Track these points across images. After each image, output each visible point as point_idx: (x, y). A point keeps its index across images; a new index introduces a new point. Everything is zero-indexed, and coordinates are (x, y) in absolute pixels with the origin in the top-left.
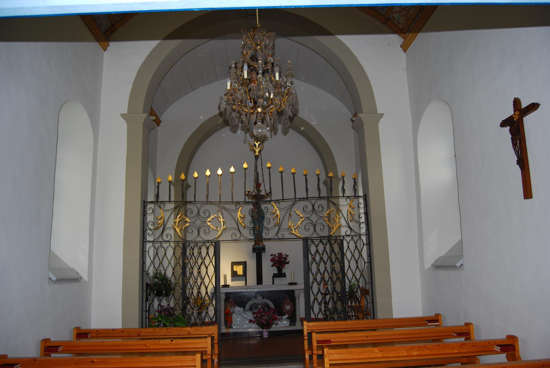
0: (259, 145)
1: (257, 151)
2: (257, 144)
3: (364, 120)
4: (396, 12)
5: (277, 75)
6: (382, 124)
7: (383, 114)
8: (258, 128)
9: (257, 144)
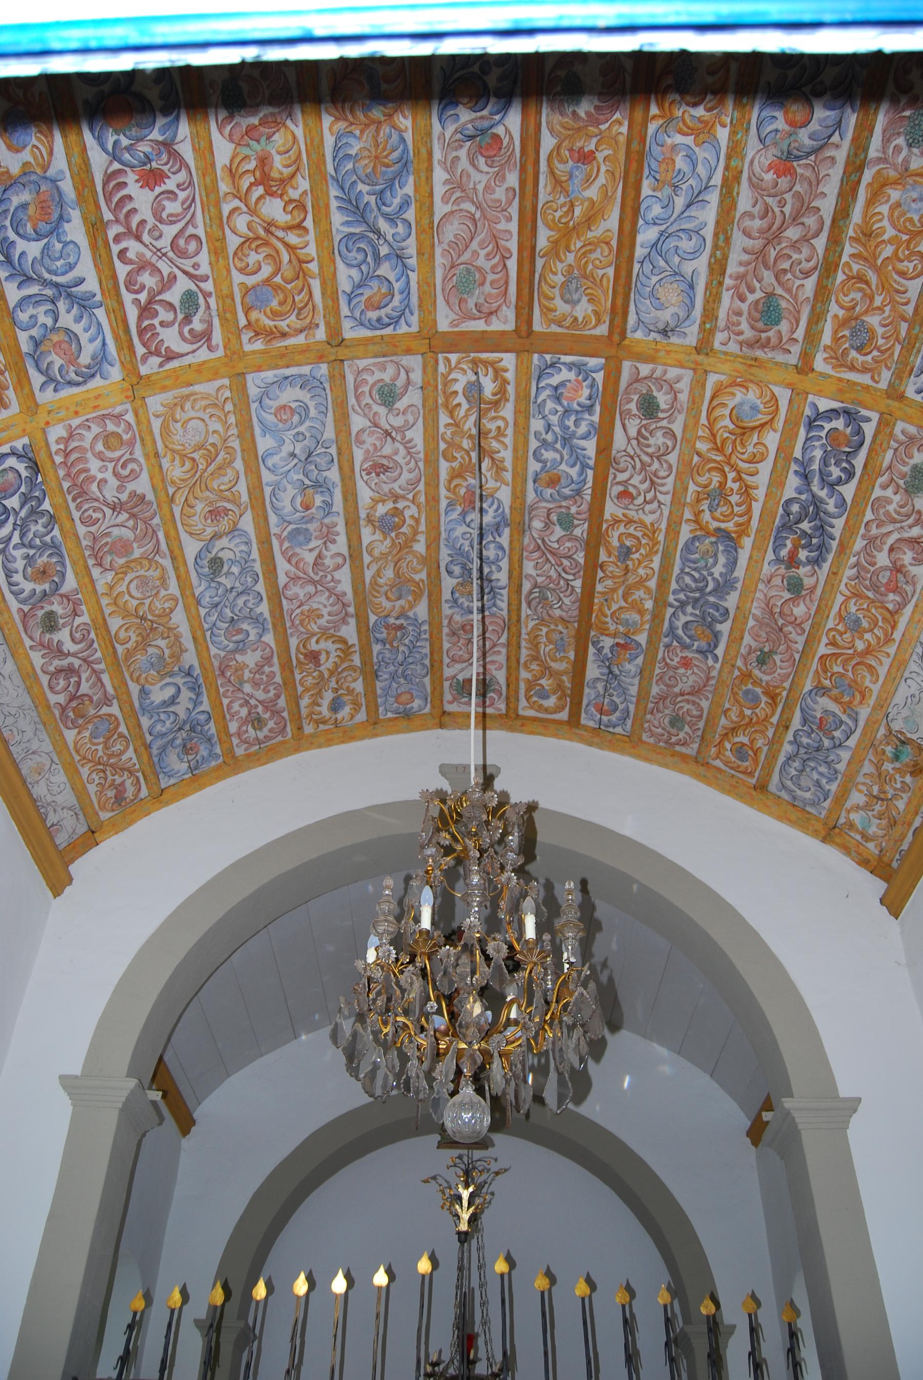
0: (472, 1196)
1: (465, 1216)
2: (465, 1194)
3: (800, 1119)
4: (858, 808)
5: (530, 923)
6: (858, 1132)
7: (859, 1100)
8: (462, 1106)
9: (465, 1194)
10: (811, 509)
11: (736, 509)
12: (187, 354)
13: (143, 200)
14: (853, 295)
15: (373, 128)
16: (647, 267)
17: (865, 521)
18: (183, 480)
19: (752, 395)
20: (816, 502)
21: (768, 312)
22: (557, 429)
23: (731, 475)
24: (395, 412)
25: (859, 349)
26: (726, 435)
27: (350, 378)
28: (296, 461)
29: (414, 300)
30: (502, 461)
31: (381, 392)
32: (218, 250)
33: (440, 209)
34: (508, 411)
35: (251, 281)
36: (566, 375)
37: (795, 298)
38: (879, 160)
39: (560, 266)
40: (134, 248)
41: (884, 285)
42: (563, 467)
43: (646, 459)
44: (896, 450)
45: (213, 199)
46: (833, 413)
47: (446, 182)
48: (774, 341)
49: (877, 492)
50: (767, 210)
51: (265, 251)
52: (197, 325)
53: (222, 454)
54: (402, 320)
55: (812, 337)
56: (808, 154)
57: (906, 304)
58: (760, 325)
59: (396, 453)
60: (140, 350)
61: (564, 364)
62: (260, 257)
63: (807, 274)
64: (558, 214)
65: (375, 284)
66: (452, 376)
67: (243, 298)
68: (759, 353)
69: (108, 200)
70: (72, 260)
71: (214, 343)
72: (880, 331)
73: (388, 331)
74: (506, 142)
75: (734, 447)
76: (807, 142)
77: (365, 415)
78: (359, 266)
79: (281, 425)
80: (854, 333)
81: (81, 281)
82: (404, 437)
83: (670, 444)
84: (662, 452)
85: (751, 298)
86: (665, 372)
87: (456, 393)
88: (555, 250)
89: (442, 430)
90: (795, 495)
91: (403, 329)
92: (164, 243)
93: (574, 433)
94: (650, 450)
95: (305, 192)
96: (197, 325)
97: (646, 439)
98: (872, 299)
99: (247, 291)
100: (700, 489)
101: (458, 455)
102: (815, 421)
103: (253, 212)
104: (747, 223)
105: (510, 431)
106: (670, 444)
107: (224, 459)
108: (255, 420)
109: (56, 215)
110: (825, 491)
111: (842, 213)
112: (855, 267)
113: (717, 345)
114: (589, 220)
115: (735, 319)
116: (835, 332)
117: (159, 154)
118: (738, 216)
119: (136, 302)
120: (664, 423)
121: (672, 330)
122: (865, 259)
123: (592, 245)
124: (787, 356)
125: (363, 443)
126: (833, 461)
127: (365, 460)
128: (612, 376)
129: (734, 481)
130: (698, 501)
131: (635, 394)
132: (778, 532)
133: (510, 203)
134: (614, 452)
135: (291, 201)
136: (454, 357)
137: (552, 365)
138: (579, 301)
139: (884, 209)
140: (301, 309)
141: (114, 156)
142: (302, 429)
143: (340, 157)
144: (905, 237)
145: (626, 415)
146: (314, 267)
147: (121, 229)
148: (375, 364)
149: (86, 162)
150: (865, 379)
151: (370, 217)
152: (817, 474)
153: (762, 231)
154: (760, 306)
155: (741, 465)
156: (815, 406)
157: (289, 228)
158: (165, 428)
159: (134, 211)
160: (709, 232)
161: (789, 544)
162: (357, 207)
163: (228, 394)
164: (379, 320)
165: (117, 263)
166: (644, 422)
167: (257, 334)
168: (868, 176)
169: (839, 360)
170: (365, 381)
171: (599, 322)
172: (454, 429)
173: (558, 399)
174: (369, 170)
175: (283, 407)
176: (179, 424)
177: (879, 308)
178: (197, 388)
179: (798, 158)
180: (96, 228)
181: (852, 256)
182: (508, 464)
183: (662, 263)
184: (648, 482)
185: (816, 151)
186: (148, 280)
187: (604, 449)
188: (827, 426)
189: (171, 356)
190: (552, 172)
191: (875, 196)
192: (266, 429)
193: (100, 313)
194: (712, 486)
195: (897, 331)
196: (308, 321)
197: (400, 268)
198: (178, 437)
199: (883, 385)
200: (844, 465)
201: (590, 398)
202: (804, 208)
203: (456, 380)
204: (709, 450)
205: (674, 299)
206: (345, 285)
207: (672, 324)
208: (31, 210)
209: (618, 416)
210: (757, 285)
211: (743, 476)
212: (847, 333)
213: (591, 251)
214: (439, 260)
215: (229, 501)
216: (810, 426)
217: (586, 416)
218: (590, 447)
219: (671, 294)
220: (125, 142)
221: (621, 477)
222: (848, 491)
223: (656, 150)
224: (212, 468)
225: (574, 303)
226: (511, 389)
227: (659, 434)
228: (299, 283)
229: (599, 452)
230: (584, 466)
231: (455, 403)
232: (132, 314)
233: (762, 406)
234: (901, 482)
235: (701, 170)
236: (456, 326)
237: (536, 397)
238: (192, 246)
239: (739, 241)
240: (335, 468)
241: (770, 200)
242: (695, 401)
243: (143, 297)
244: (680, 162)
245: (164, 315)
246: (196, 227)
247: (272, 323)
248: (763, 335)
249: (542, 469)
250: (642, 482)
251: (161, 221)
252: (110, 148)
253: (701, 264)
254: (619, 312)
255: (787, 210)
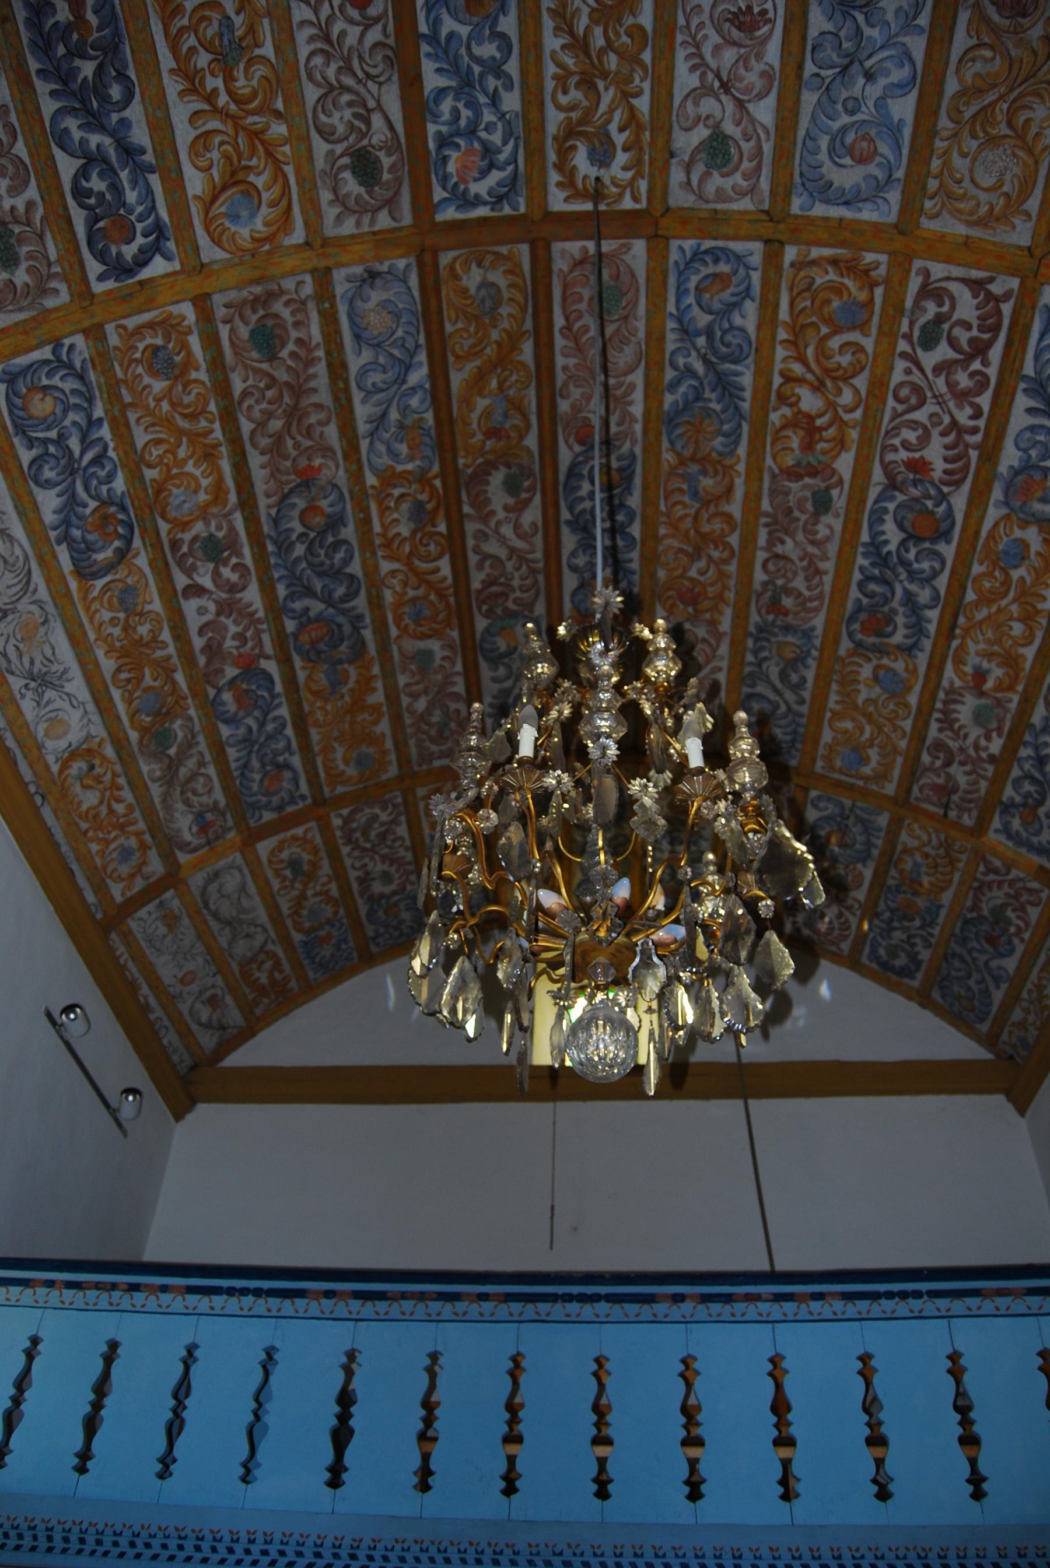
10: (95, 104)
11: (192, 41)
12: (956, 279)
13: (935, 454)
14: (192, 397)
15: (699, 456)
16: (410, 344)
17: (20, 138)
18: (1040, 96)
19: (244, 233)
20: (95, 122)
21: (268, 339)
22: (483, 99)
23: (223, 99)
24: (711, 122)
25: (155, 349)
26: (254, 162)
27: (764, 184)
28: (868, 64)
29: (672, 280)
30: (557, 29)
31: (726, 156)
32: (879, 386)
33: (637, 378)
34: (554, 119)
35: (854, 336)
36: (480, 188)
37: (246, 366)
38: (230, 513)
39: (506, 324)
40: (963, 416)
41: (168, 422)
42: (464, 31)
43: (348, 81)
44: (49, 264)
45: (869, 426)
46: (143, 260)
47: (631, 403)
48: (248, 312)
49: (32, 192)
50: (308, 433)
51: (831, 364)
52: (931, 309)
53: (967, 115)
54: (688, 255)
55: (211, 341)
56: (291, 491)
57: (138, 420)
58: (270, 322)
59: (717, 49)
60: (1007, 308)
61: (485, 203)
62: (837, 358)
63: (245, 394)
64: (514, 378)
65: (716, 305)
66: (629, 174)
67: (869, 320)
68: (258, 290)
69: (967, 466)
70: (1028, 434)
71: (920, 279)
72: (147, 380)
73: (708, 244)
74: (572, 439)
75: (236, 148)
76: (296, 500)
77: (753, 121)
78: (732, 328)
79: (873, 132)
80: (170, 363)
81: (1030, 411)
82: (703, 77)
83: (322, 117)
84: (329, 101)
85: (291, 347)
86: (358, 224)
87: (625, 149)
88: (513, 341)
89: (646, 86)
90: (127, 113)
91: (688, 244)
92: (930, 407)
93: (456, 99)
94: (346, 97)
95: (775, 409)
96: (931, 309)
97: (356, 116)
98: (172, 404)
99: (863, 327)
100: (257, 52)
101: (625, 39)
102: (157, 239)
103: (832, 405)
104: (322, 416)
105: (550, 85)
106: (322, 117)
107: (967, 104)
108: (905, 151)
109: (1020, 478)
110: (93, 146)
111: (241, 466)
112: (203, 423)
113: (308, 278)
114: (481, 376)
115: (299, 317)
116: (189, 353)
117: (903, 482)
118: (334, 419)
119: (986, 363)
120: (339, 149)
121: (364, 281)
122: (198, 435)
123: (474, 352)
124: (226, 300)
125: (763, 74)
126: (108, 197)
127: (765, 40)
128: (423, 206)
129: (215, 90)
130: (251, 29)
131: (388, 182)
132: (116, 33)
133: (565, 384)
134: (395, 77)
135: (791, 405)
136: (628, 204)
137: (500, 199)
138: (479, 288)
139: (205, 483)
140: (808, 289)
141: (943, 497)
142: (845, 119)
143: (734, 437)
144: (175, 471)
145: (393, 146)
146: (782, 335)
147: (968, 438)
148: (730, 200)
149: (970, 503)
150: (131, 323)
151: (712, 377)
152: (116, 165)
153: (307, 414)
154: (277, 342)
155: (214, 124)
156: (168, 258)
157: (800, 381)
158: (1025, 193)
159: (947, 447)
160: (357, 396)
161: (93, 20)
162: (724, 389)
163: (928, 204)
164: (716, 261)
165: (986, 408)
166: (365, 142)
167: (866, 272)
168: (233, 498)
169: (169, 326)
170: (746, 177)
171: (451, 267)
172: (631, 88)
173: (488, 150)
174: (707, 422)
175: (862, 160)
176: (1005, 189)
177: (161, 400)
178: (962, 230)
179: (298, 486)
180: (990, 453)
181: (212, 431)
182: (548, 24)
183: (396, 352)
184: (334, 36)
185: (285, 497)
186: (963, 380)
187: (411, 81)
188: (140, 240)
189: (976, 286)
190: (525, 417)
191: (218, 491)
192: (894, 131)
193: (1029, 369)
194: (242, 66)
195: (131, 390)
196: (802, 274)
197: (686, 319)
198: (1016, 170)
199: (110, 328)
200: (92, 201)
201: (445, 160)
202: (276, 449)
203: (625, 168)
204: (267, 127)
205: (373, 318)
206: (751, 308)
207: (366, 288)
208: (1039, 494)
209: (403, 140)
210: (289, 362)
211: (207, 107)
212: (178, 359)
213: (474, 346)
214: (641, 325)
215: (988, 22)
216: (158, 228)
217: (444, 129)
218: (432, 79)
219: (377, 322)
220: (929, 504)
221: (374, 35)
222: (67, 166)
223: (428, 452)
224: (991, 97)
225: (484, 284)
226: (552, 157)
227: (341, 129)
228: (803, 320)
229: (418, 77)
230: (433, 38)
231: (627, 133)
232: (996, 353)
233: (227, 224)
234: (17, 229)
235: (382, 448)
236: (623, 246)
237: (516, 147)
238: (904, 392)
239: (324, 396)
240: (813, 33)
241: (309, 443)
242: (311, 206)
243: (976, 365)
244: (403, 449)
245: (963, 336)
246: (894, 409)
247: (846, 281)
248: (261, 313)
249: (496, 19)
250: (343, 34)
251: (925, 428)
252: (944, 505)
253: (355, 363)
254: (431, 288)
255: (290, 443)
